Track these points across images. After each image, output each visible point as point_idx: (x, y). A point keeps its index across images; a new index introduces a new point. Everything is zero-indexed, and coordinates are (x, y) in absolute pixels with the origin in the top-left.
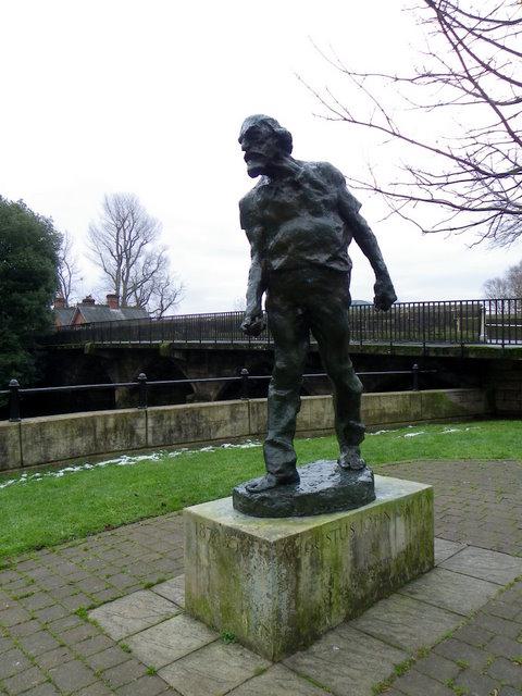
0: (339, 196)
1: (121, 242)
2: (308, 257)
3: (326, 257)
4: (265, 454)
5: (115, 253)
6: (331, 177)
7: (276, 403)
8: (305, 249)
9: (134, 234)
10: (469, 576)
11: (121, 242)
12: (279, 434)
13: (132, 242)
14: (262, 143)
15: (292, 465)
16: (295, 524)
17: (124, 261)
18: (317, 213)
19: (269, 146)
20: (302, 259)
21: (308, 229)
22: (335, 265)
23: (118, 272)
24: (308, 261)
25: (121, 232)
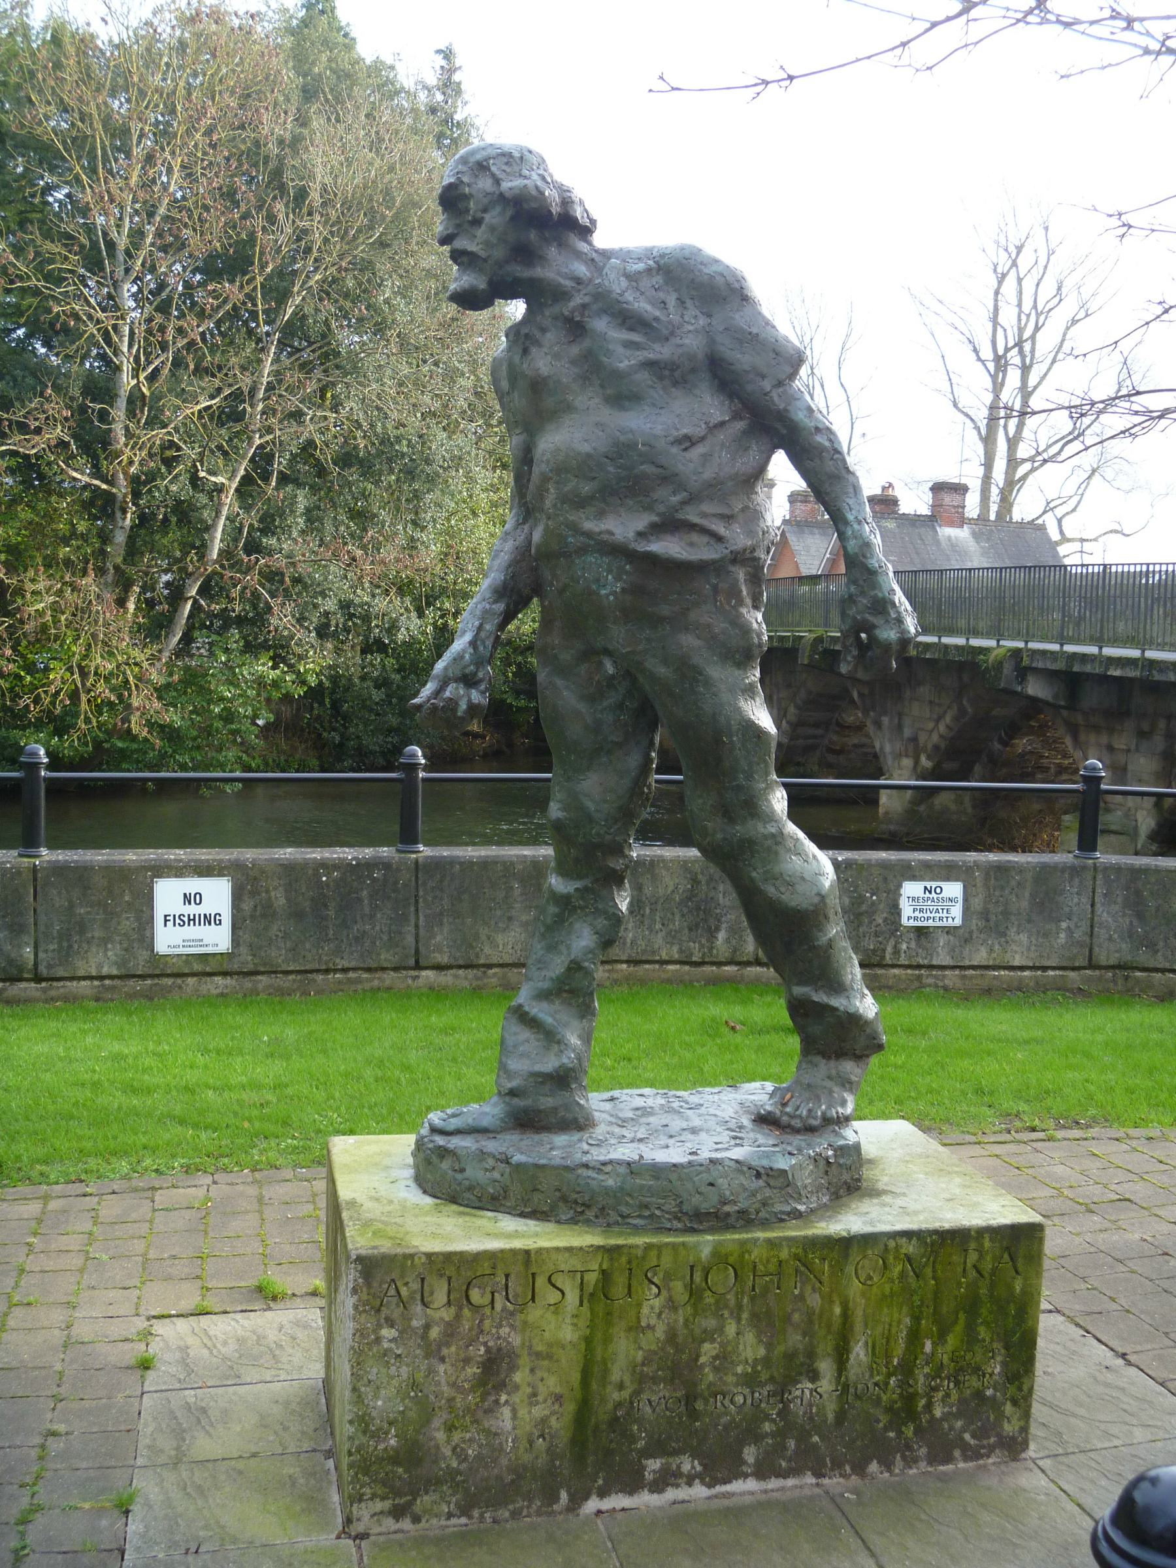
0: (712, 342)
1: (1008, 317)
2: (588, 525)
3: (642, 521)
4: (503, 1042)
5: (987, 353)
6: (701, 284)
7: (553, 909)
8: (580, 503)
9: (1047, 290)
10: (1109, 1411)
11: (1008, 317)
12: (544, 995)
13: (1041, 314)
14: (477, 222)
15: (563, 1079)
16: (579, 1234)
17: (1013, 377)
18: (622, 396)
19: (492, 229)
20: (575, 528)
21: (586, 448)
22: (670, 547)
23: (993, 408)
24: (588, 535)
25: (1010, 284)
